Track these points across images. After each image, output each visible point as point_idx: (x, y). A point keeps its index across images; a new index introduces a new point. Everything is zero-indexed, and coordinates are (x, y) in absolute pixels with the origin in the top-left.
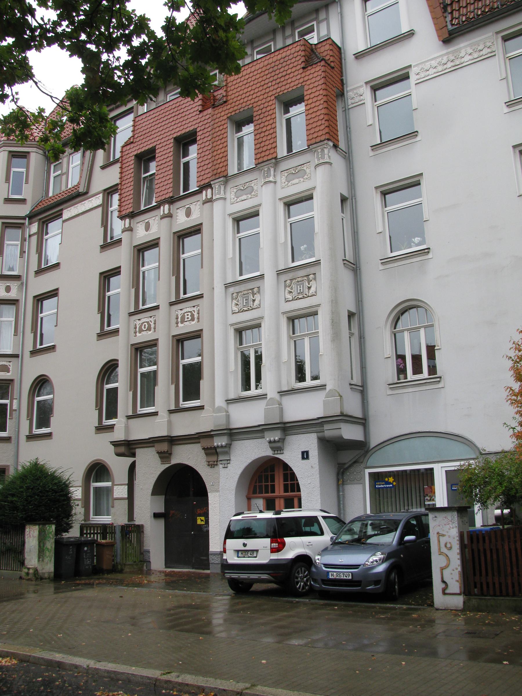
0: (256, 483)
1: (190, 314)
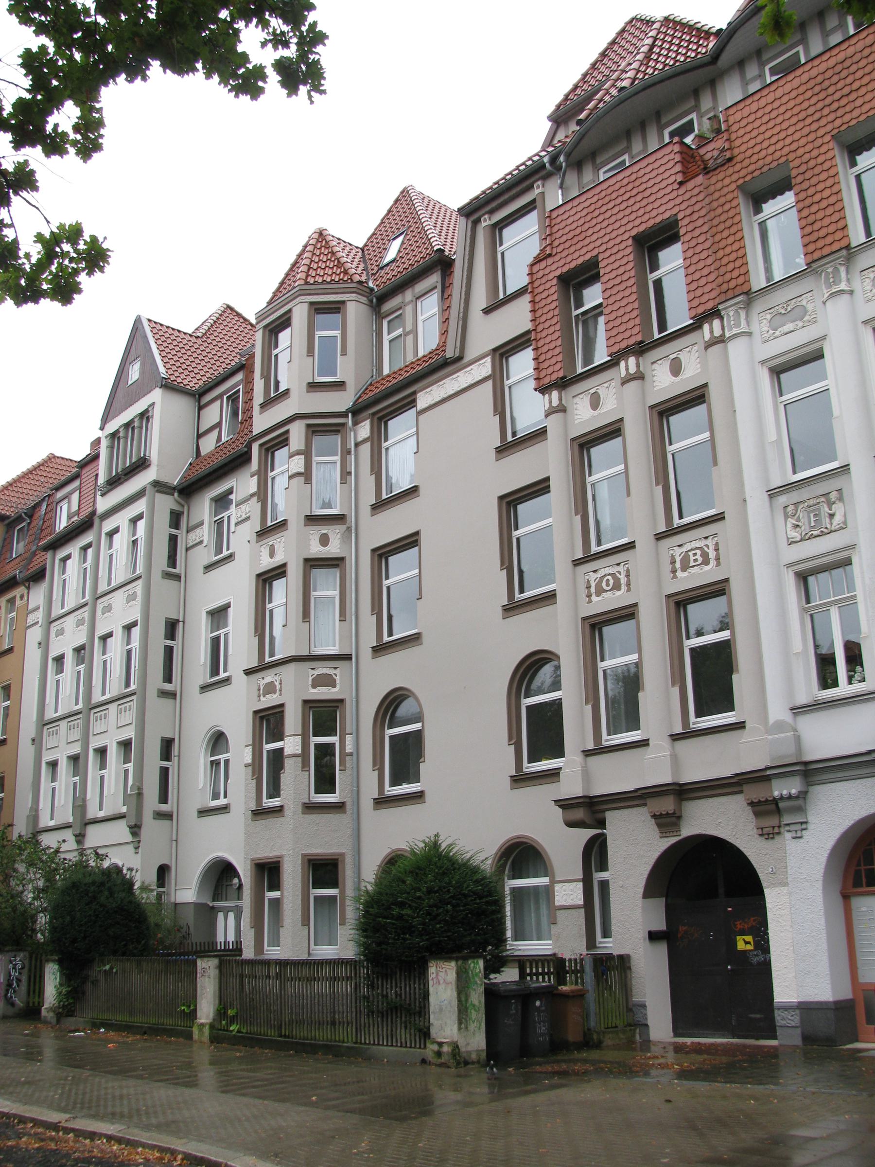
0: (859, 864)
1: (699, 552)
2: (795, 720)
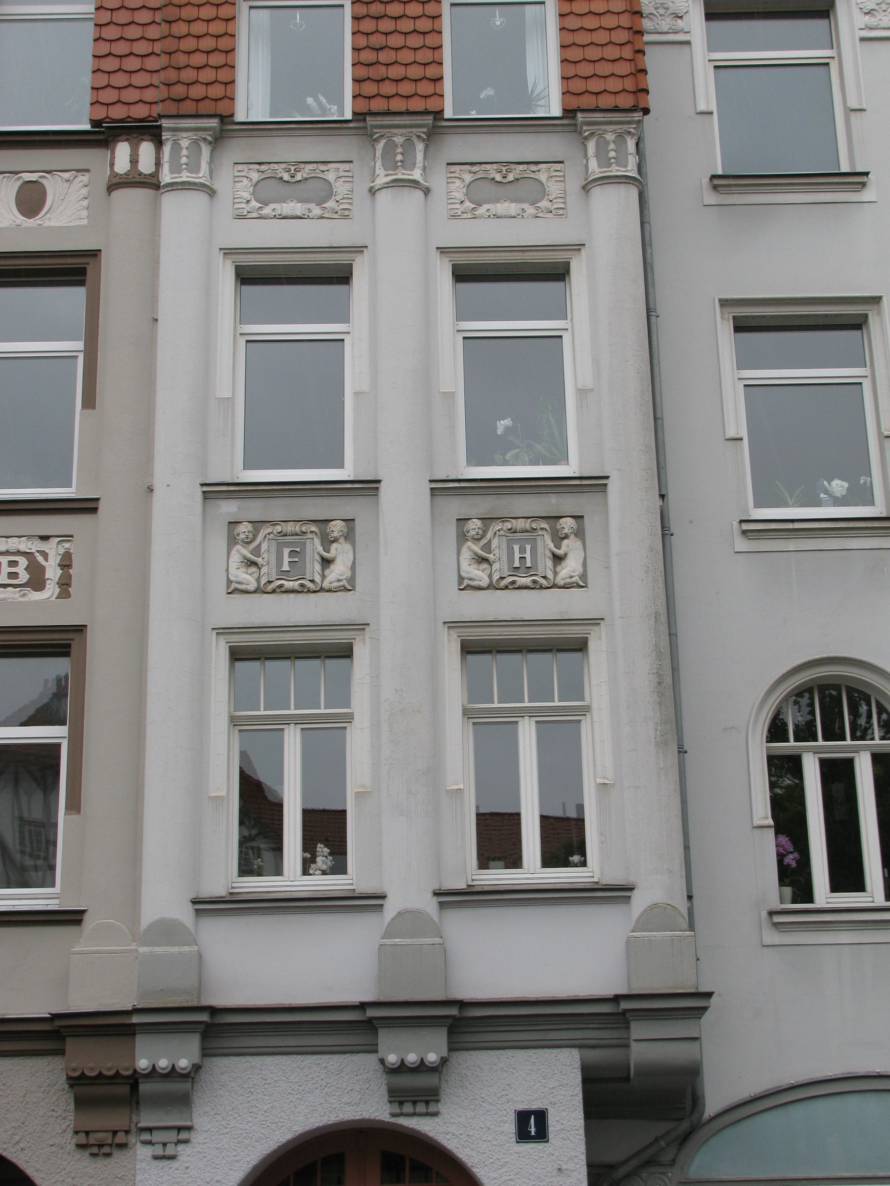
2: (196, 925)
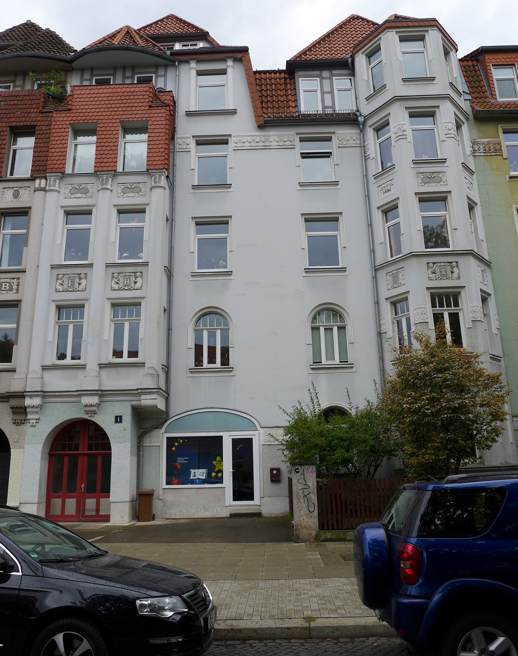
1: (8, 284)
